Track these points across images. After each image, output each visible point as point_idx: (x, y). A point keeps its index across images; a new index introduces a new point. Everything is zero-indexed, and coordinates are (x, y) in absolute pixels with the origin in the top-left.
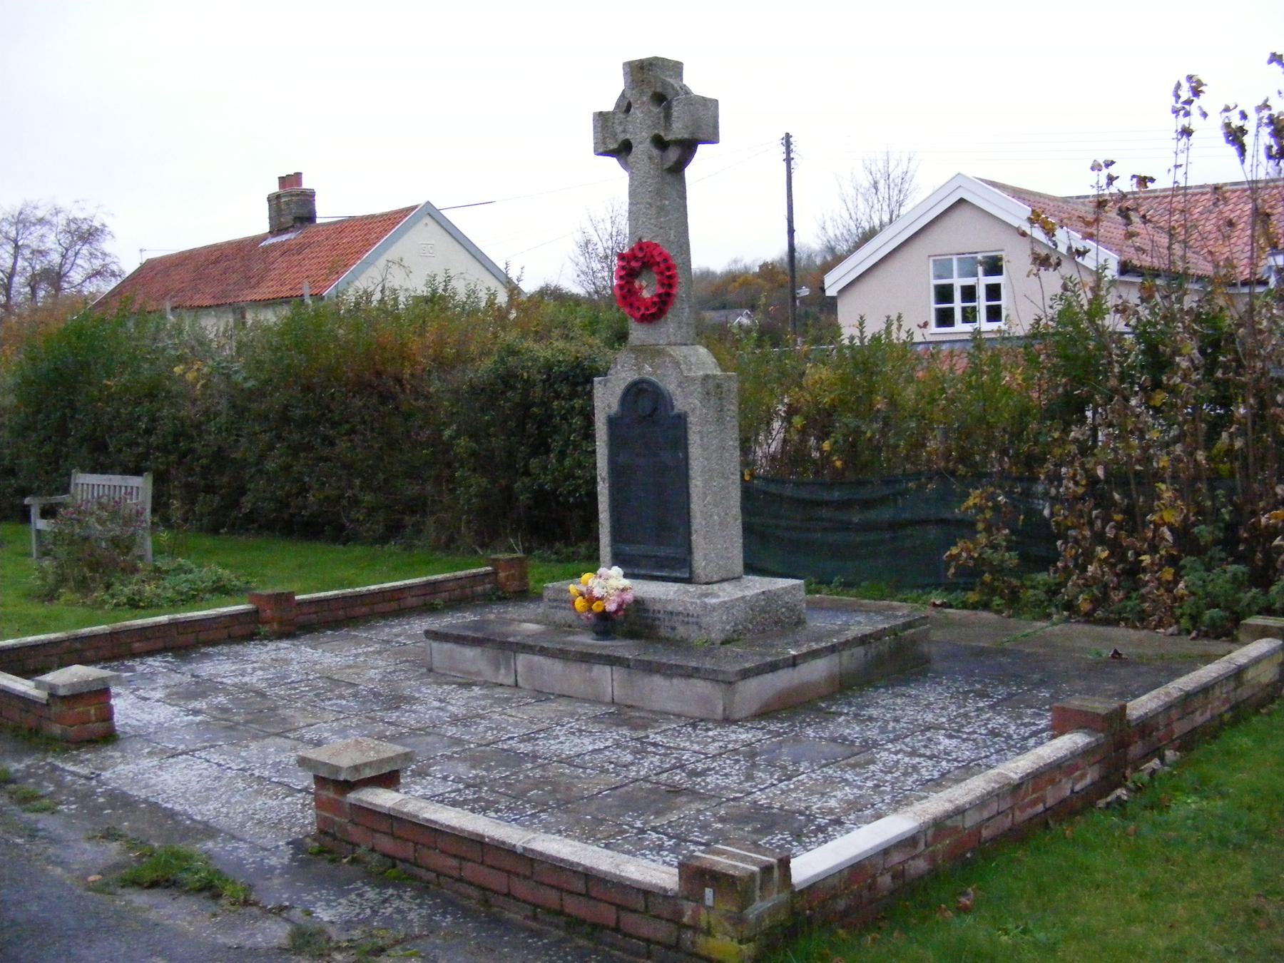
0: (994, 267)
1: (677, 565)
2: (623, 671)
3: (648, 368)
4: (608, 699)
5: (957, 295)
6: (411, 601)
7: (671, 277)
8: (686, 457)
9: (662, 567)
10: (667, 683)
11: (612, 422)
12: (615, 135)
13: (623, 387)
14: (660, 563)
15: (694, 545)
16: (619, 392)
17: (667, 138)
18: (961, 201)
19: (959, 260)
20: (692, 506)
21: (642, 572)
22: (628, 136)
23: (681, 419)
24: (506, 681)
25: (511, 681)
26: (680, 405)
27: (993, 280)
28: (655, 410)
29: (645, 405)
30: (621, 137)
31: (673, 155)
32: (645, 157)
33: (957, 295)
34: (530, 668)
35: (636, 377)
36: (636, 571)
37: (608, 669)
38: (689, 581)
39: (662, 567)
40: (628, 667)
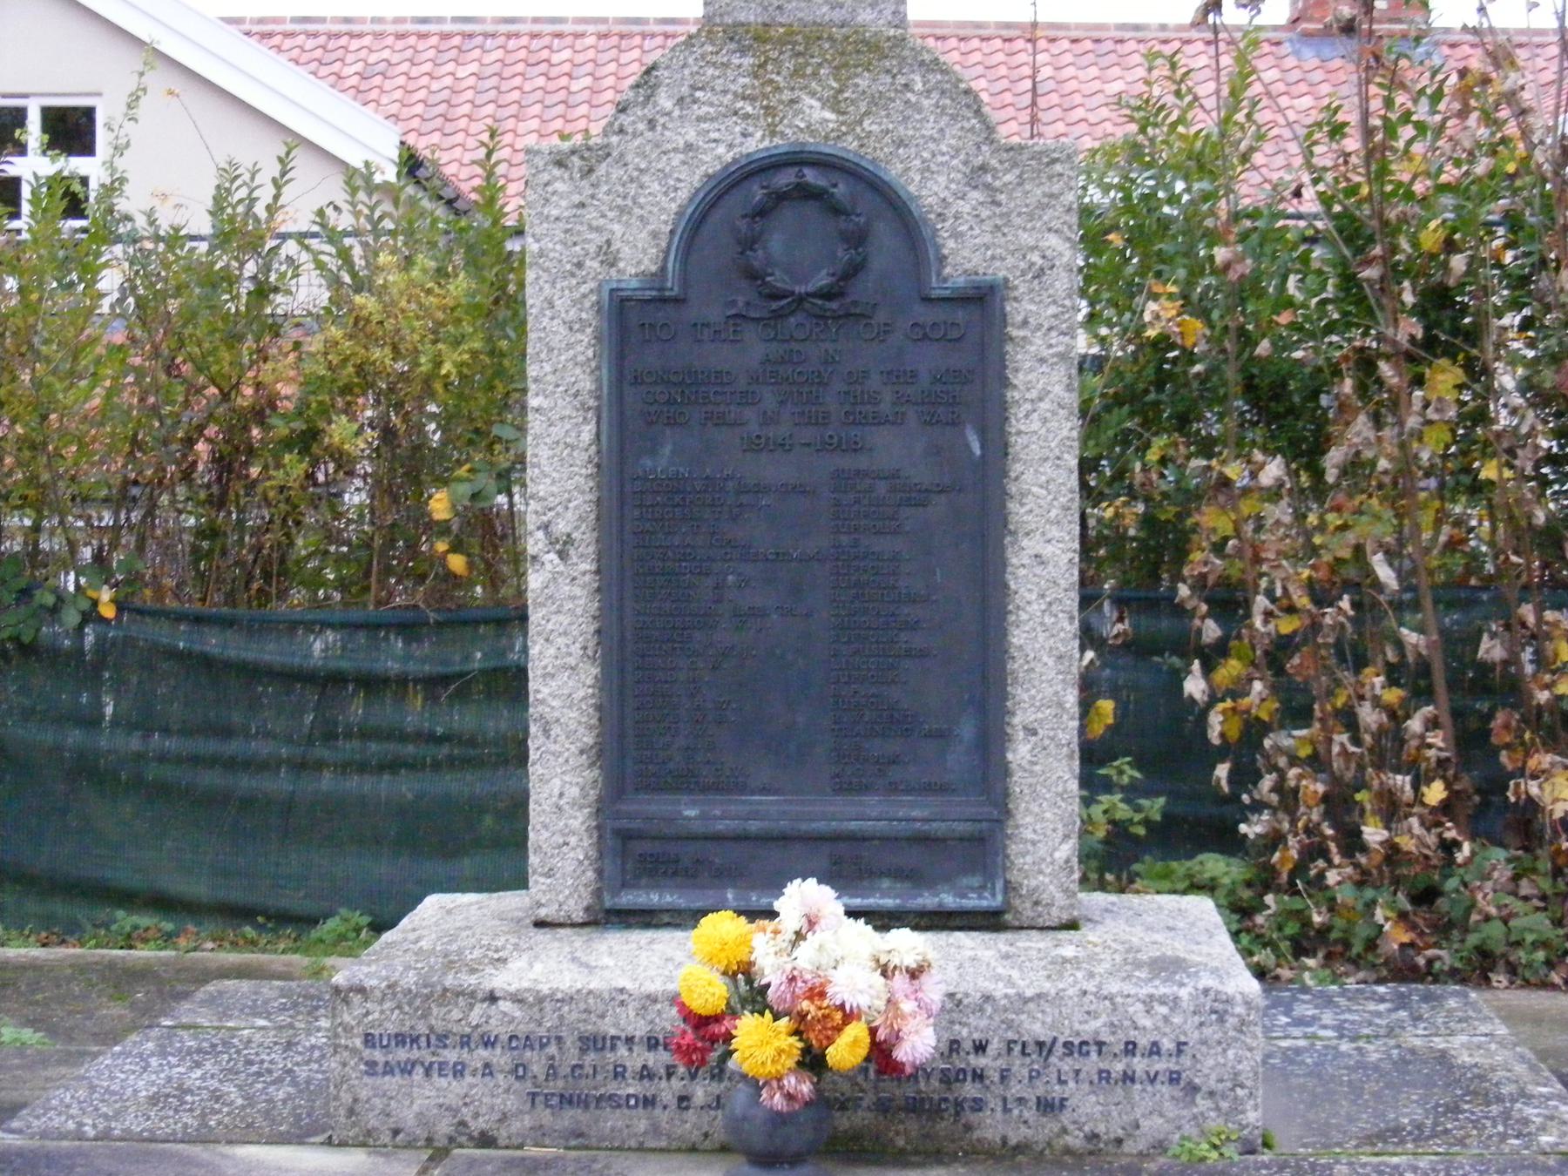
6: (980, 921)
11: (631, 321)
13: (689, 181)
15: (1019, 782)
23: (983, 300)
26: (965, 253)
29: (798, 253)
35: (756, 143)
38: (990, 921)
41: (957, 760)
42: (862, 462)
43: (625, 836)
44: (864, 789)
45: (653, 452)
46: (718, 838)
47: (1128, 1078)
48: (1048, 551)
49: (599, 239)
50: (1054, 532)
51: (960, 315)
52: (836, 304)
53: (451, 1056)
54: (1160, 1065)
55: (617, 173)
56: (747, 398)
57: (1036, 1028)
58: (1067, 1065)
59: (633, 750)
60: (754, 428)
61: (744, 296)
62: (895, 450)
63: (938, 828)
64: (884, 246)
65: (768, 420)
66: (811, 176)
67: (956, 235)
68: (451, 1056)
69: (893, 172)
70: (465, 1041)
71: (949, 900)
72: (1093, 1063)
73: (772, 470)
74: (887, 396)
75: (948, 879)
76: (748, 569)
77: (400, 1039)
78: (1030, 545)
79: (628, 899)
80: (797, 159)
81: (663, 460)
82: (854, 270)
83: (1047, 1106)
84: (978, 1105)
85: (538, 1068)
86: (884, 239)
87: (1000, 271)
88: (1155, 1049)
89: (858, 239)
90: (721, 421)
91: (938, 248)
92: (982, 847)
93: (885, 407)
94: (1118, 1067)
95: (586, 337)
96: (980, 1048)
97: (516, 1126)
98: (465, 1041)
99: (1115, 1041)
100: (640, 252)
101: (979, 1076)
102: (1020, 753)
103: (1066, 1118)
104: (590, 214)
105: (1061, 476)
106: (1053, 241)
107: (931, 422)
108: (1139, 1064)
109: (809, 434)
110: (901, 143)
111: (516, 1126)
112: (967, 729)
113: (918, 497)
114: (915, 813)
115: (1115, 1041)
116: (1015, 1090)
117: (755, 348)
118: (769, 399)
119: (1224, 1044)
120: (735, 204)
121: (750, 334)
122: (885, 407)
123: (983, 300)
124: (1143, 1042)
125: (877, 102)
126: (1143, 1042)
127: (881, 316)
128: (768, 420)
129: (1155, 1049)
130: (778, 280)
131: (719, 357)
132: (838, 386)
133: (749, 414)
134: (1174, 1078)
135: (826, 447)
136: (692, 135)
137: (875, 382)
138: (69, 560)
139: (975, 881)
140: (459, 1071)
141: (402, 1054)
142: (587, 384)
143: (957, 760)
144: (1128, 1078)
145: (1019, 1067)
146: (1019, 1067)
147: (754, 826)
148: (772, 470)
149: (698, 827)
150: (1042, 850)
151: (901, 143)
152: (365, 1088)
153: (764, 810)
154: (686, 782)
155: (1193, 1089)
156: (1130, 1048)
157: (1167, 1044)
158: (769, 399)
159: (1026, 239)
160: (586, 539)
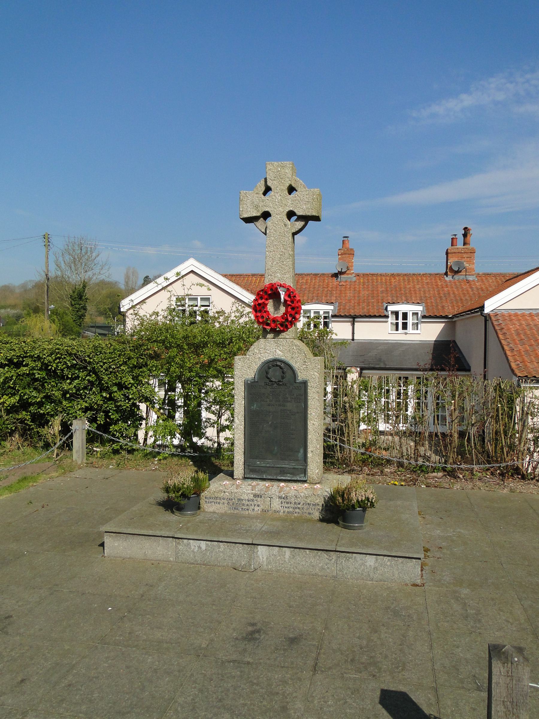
15: (309, 460)
20: (309, 437)
23: (305, 383)
26: (301, 376)
45: (253, 406)
53: (218, 501)
62: (290, 406)
63: (297, 467)
64: (289, 374)
66: (279, 363)
79: (248, 476)
80: (275, 360)
81: (255, 407)
82: (283, 378)
83: (309, 514)
85: (231, 504)
93: (289, 399)
96: (299, 504)
102: (309, 455)
114: (293, 465)
123: (305, 383)
133: (268, 400)
135: (280, 405)
138: (378, 410)
142: (309, 415)
145: (305, 507)
146: (305, 507)
154: (257, 458)
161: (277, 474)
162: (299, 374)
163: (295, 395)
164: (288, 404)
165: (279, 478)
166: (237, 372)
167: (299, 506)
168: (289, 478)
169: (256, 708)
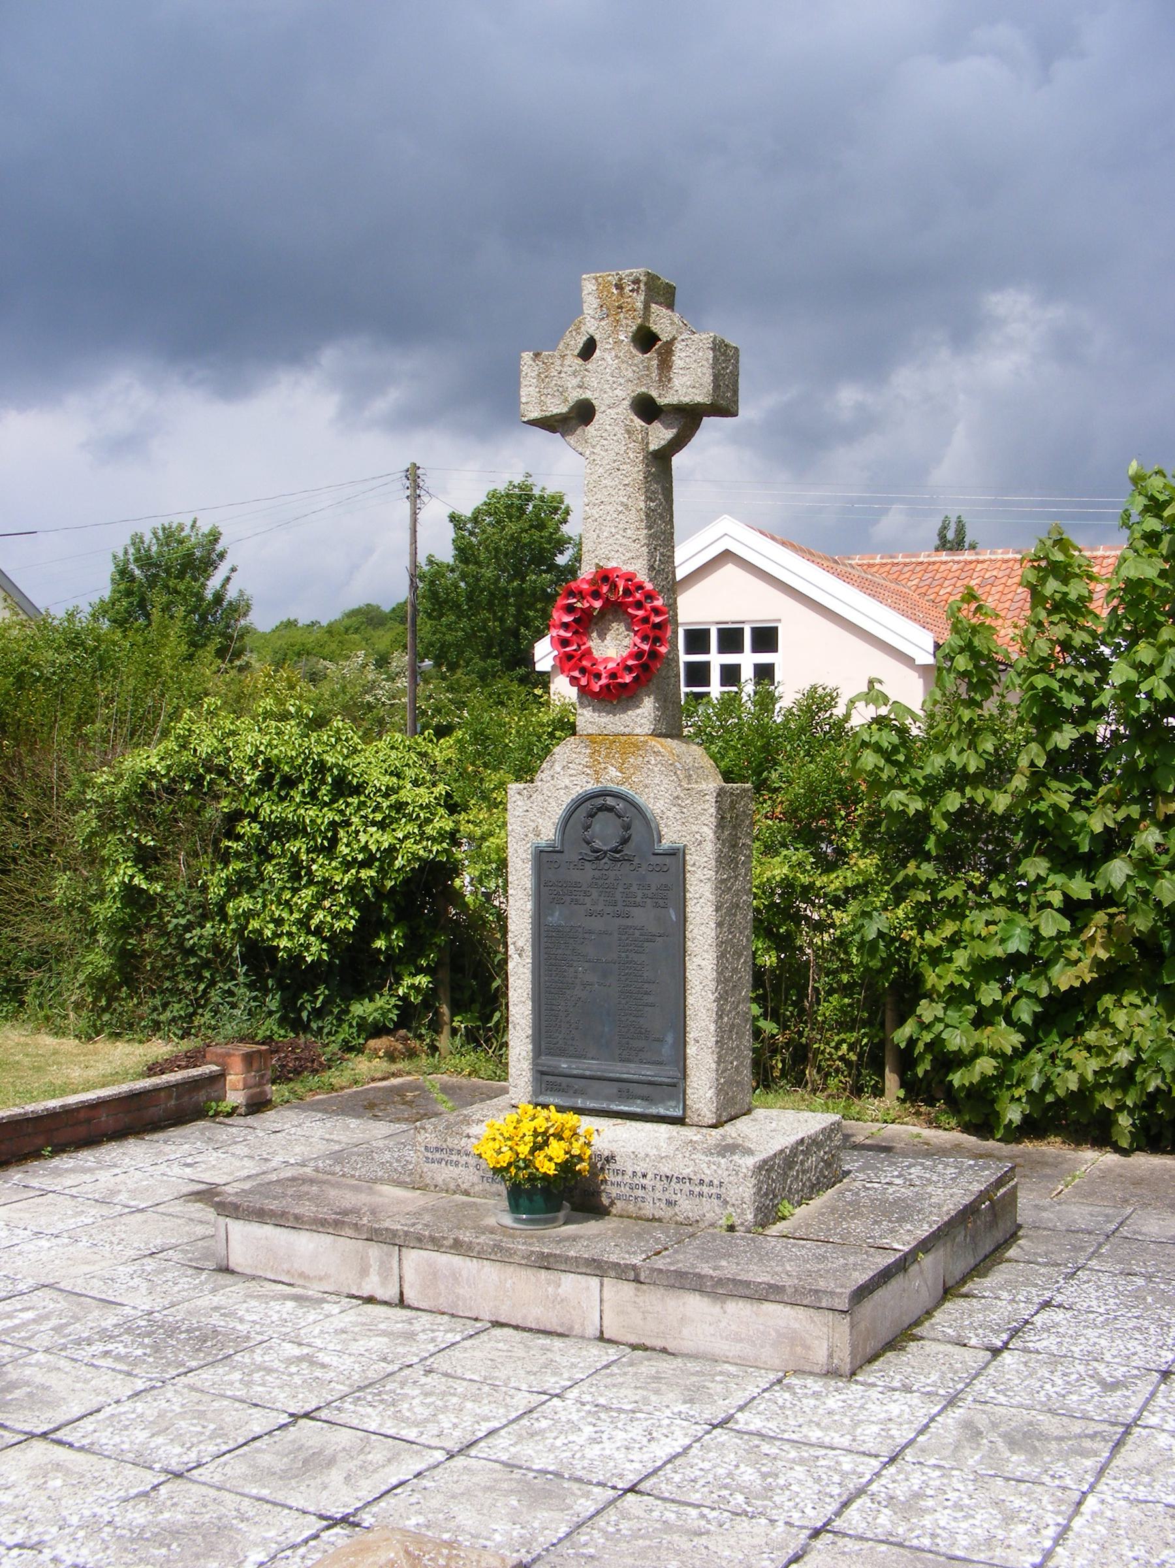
0: (766, 639)
1: (656, 1095)
2: (628, 1289)
3: (613, 772)
4: (592, 1330)
5: (715, 675)
6: (104, 1119)
7: (659, 626)
8: (683, 919)
9: (629, 1097)
10: (716, 1309)
11: (543, 858)
12: (562, 391)
13: (567, 800)
14: (626, 1088)
15: (690, 1062)
16: (557, 811)
17: (662, 401)
18: (726, 556)
19: (719, 630)
20: (690, 1000)
21: (591, 1104)
22: (588, 395)
23: (677, 855)
24: (380, 1294)
25: (391, 1293)
26: (671, 835)
27: (764, 658)
28: (625, 841)
29: (605, 832)
30: (575, 395)
31: (660, 435)
32: (620, 431)
33: (715, 675)
34: (434, 1276)
35: (591, 786)
36: (580, 1103)
37: (594, 1282)
38: (680, 1121)
39: (626, 1096)
40: (637, 1280)
41: (666, 1051)
42: (629, 922)
43: (543, 1073)
44: (629, 1061)
46: (575, 1076)
47: (701, 1195)
48: (703, 963)
49: (533, 825)
50: (706, 955)
51: (667, 860)
52: (618, 853)
53: (454, 1158)
54: (714, 1191)
55: (540, 797)
56: (587, 894)
57: (665, 1170)
58: (677, 1186)
59: (544, 1040)
60: (588, 906)
61: (586, 850)
62: (643, 917)
65: (595, 903)
66: (610, 801)
67: (667, 826)
68: (454, 1158)
69: (641, 800)
70: (459, 1152)
71: (662, 1111)
72: (687, 1187)
73: (596, 924)
74: (640, 894)
75: (662, 1101)
76: (586, 965)
77: (437, 1149)
78: (697, 961)
81: (555, 918)
82: (625, 841)
83: (669, 1203)
84: (643, 1200)
86: (637, 825)
87: (684, 841)
88: (711, 1184)
89: (627, 827)
90: (577, 902)
91: (659, 832)
92: (676, 1087)
94: (697, 1189)
95: (529, 865)
96: (644, 1176)
97: (477, 1188)
98: (459, 1152)
99: (696, 1179)
100: (548, 833)
101: (644, 1187)
102: (691, 1050)
103: (677, 1209)
104: (530, 814)
105: (708, 931)
106: (705, 829)
107: (657, 906)
108: (705, 1189)
109: (609, 909)
110: (646, 786)
111: (477, 1188)
112: (670, 1039)
113: (651, 937)
114: (648, 1072)
115: (696, 1179)
116: (658, 1195)
117: (588, 873)
118: (595, 894)
119: (738, 1185)
120: (582, 812)
121: (588, 865)
122: (638, 899)
123: (677, 855)
124: (707, 1180)
125: (637, 768)
126: (707, 1180)
127: (636, 861)
128: (595, 903)
129: (711, 1184)
130: (598, 844)
131: (575, 875)
132: (621, 889)
134: (719, 1197)
136: (567, 782)
137: (634, 888)
139: (673, 1103)
140: (457, 1164)
141: (438, 1155)
142: (529, 885)
143: (666, 1051)
144: (701, 1195)
147: (588, 1073)
148: (596, 924)
149: (567, 1071)
150: (701, 1092)
151: (646, 786)
152: (426, 1167)
153: (590, 1066)
154: (562, 1053)
155: (726, 1202)
156: (702, 1182)
157: (716, 1182)
158: (595, 894)
159: (695, 828)
160: (528, 949)
161: (610, 1099)
162: (664, 831)
163: (653, 890)
164: (635, 911)
165: (614, 1107)
166: (514, 825)
167: (644, 1181)
168: (639, 1110)
169: (1050, 1507)
